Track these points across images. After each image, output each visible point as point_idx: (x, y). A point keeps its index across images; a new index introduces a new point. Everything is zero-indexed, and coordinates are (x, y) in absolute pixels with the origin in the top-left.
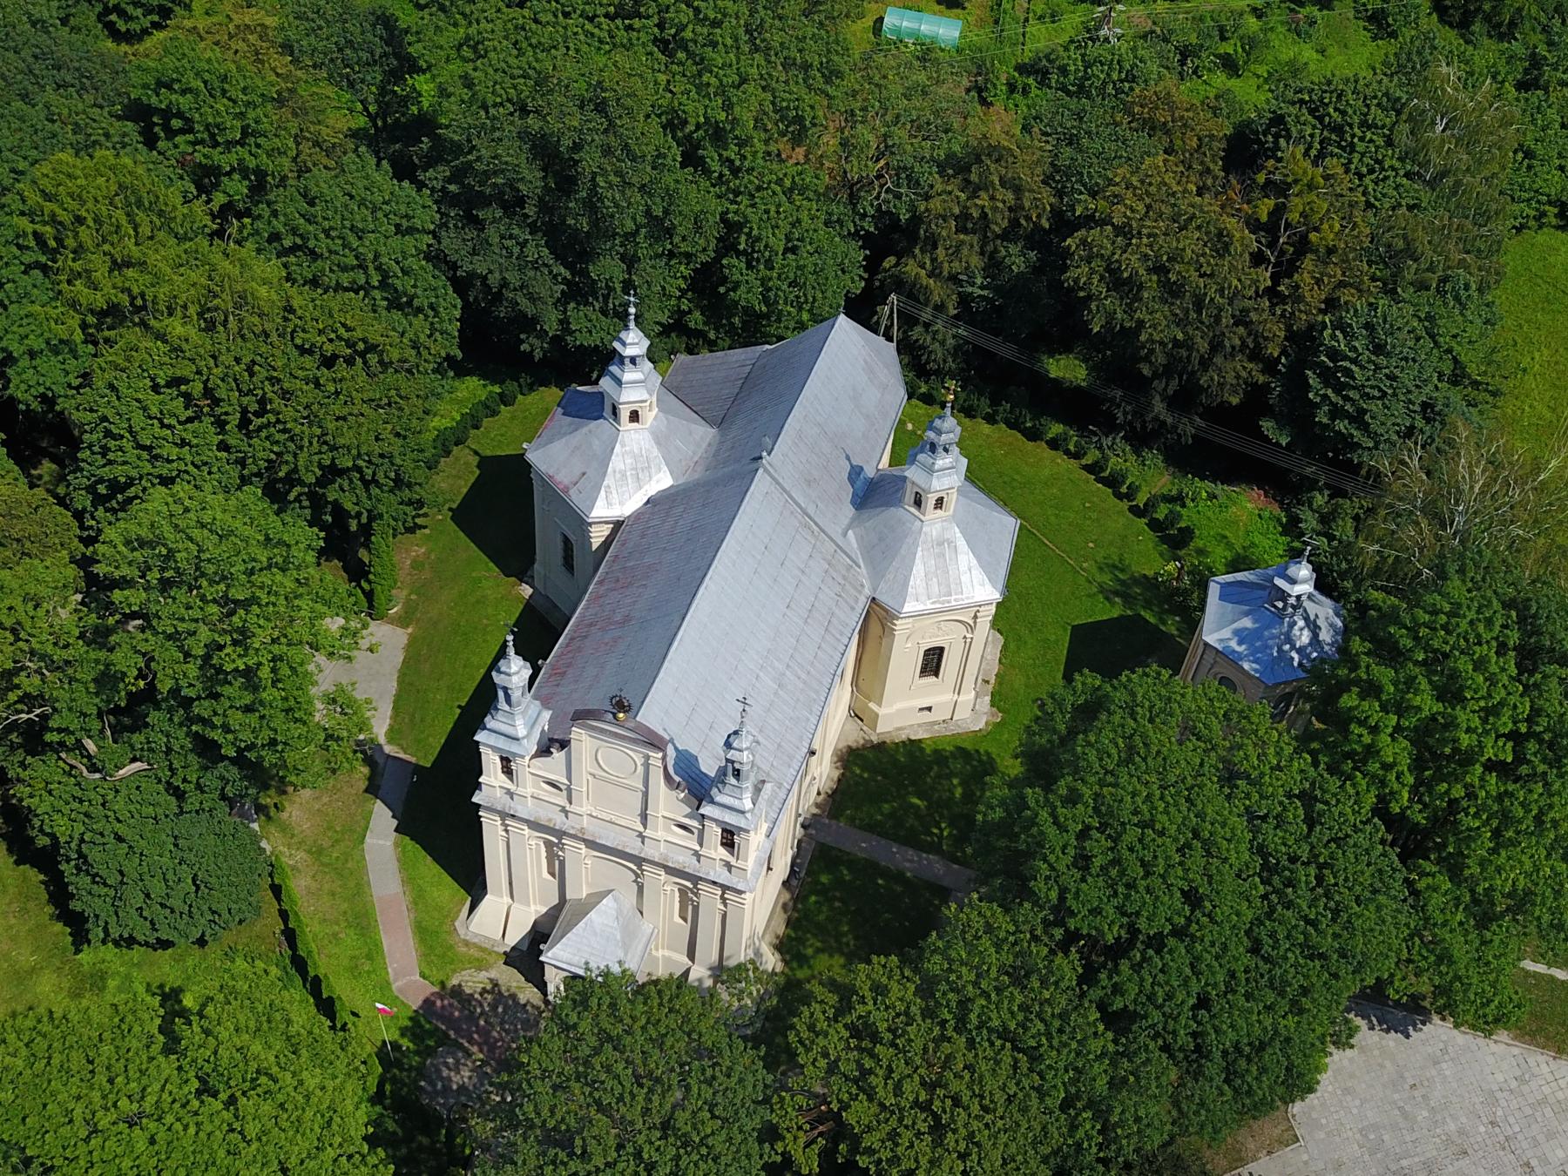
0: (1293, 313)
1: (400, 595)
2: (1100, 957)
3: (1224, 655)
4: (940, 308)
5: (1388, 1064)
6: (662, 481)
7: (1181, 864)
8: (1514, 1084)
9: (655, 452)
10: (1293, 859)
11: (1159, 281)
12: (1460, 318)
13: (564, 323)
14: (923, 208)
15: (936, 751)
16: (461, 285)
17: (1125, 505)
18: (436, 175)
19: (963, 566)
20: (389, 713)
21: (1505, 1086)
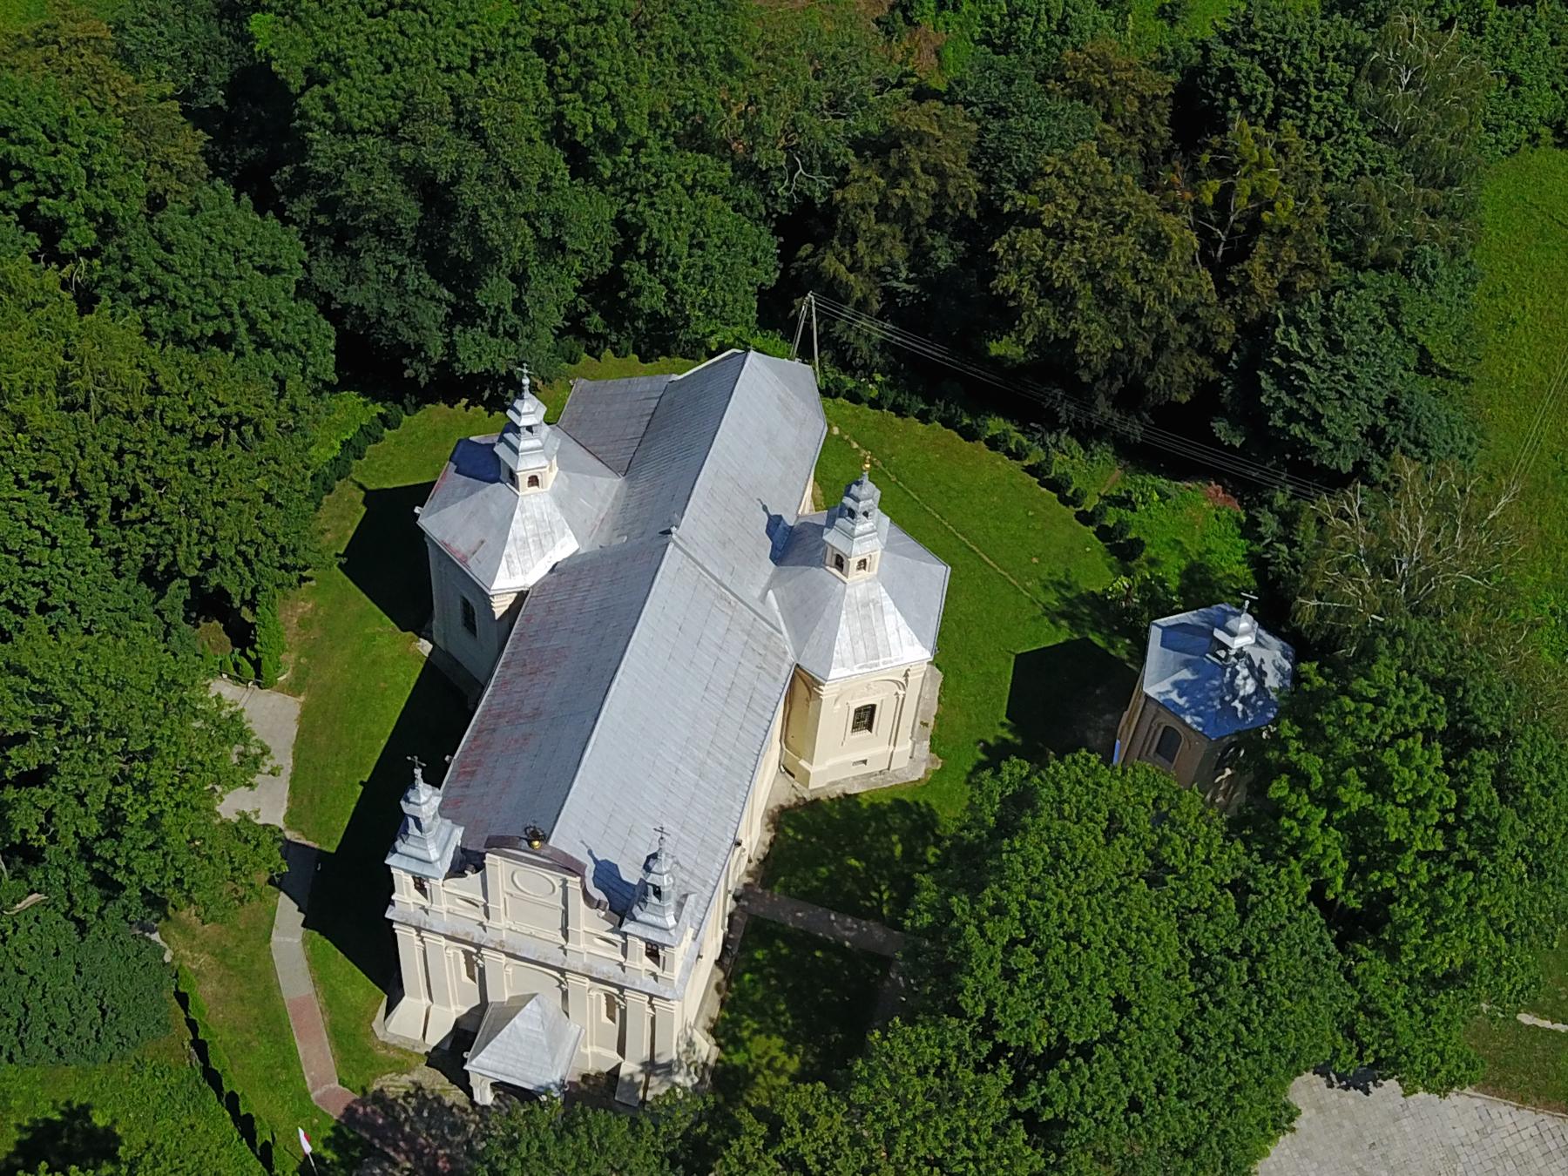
0: (1243, 306)
1: (289, 658)
2: (1029, 1067)
3: (1166, 706)
4: (862, 305)
5: (1346, 1123)
6: (566, 547)
7: (1106, 974)
8: (1475, 1138)
9: (558, 516)
10: (1227, 951)
11: (1094, 288)
12: (1428, 299)
13: (451, 347)
14: (838, 197)
15: (872, 806)
16: (335, 317)
17: (1071, 511)
18: (302, 206)
19: (890, 627)
20: (286, 794)
21: (1465, 1140)
